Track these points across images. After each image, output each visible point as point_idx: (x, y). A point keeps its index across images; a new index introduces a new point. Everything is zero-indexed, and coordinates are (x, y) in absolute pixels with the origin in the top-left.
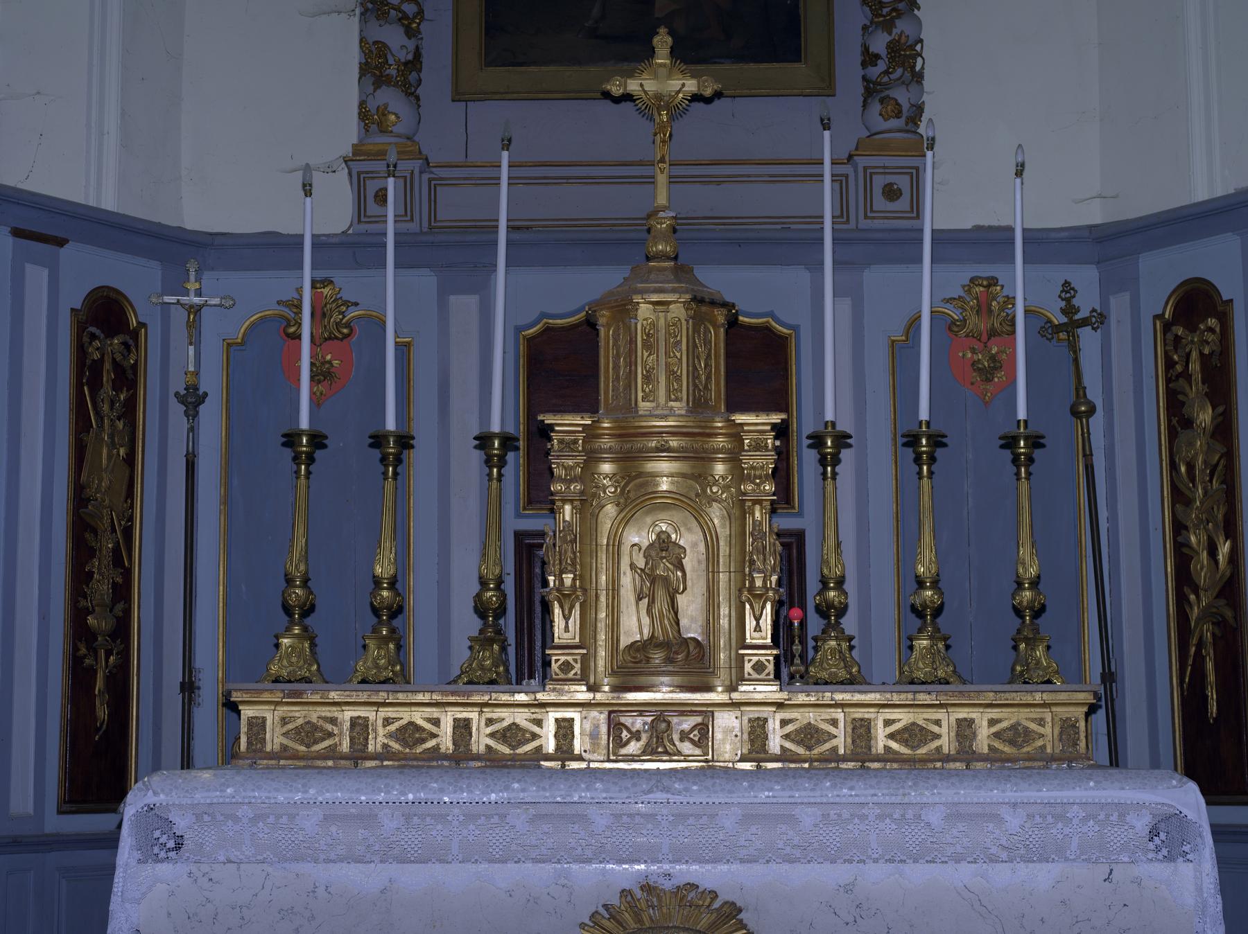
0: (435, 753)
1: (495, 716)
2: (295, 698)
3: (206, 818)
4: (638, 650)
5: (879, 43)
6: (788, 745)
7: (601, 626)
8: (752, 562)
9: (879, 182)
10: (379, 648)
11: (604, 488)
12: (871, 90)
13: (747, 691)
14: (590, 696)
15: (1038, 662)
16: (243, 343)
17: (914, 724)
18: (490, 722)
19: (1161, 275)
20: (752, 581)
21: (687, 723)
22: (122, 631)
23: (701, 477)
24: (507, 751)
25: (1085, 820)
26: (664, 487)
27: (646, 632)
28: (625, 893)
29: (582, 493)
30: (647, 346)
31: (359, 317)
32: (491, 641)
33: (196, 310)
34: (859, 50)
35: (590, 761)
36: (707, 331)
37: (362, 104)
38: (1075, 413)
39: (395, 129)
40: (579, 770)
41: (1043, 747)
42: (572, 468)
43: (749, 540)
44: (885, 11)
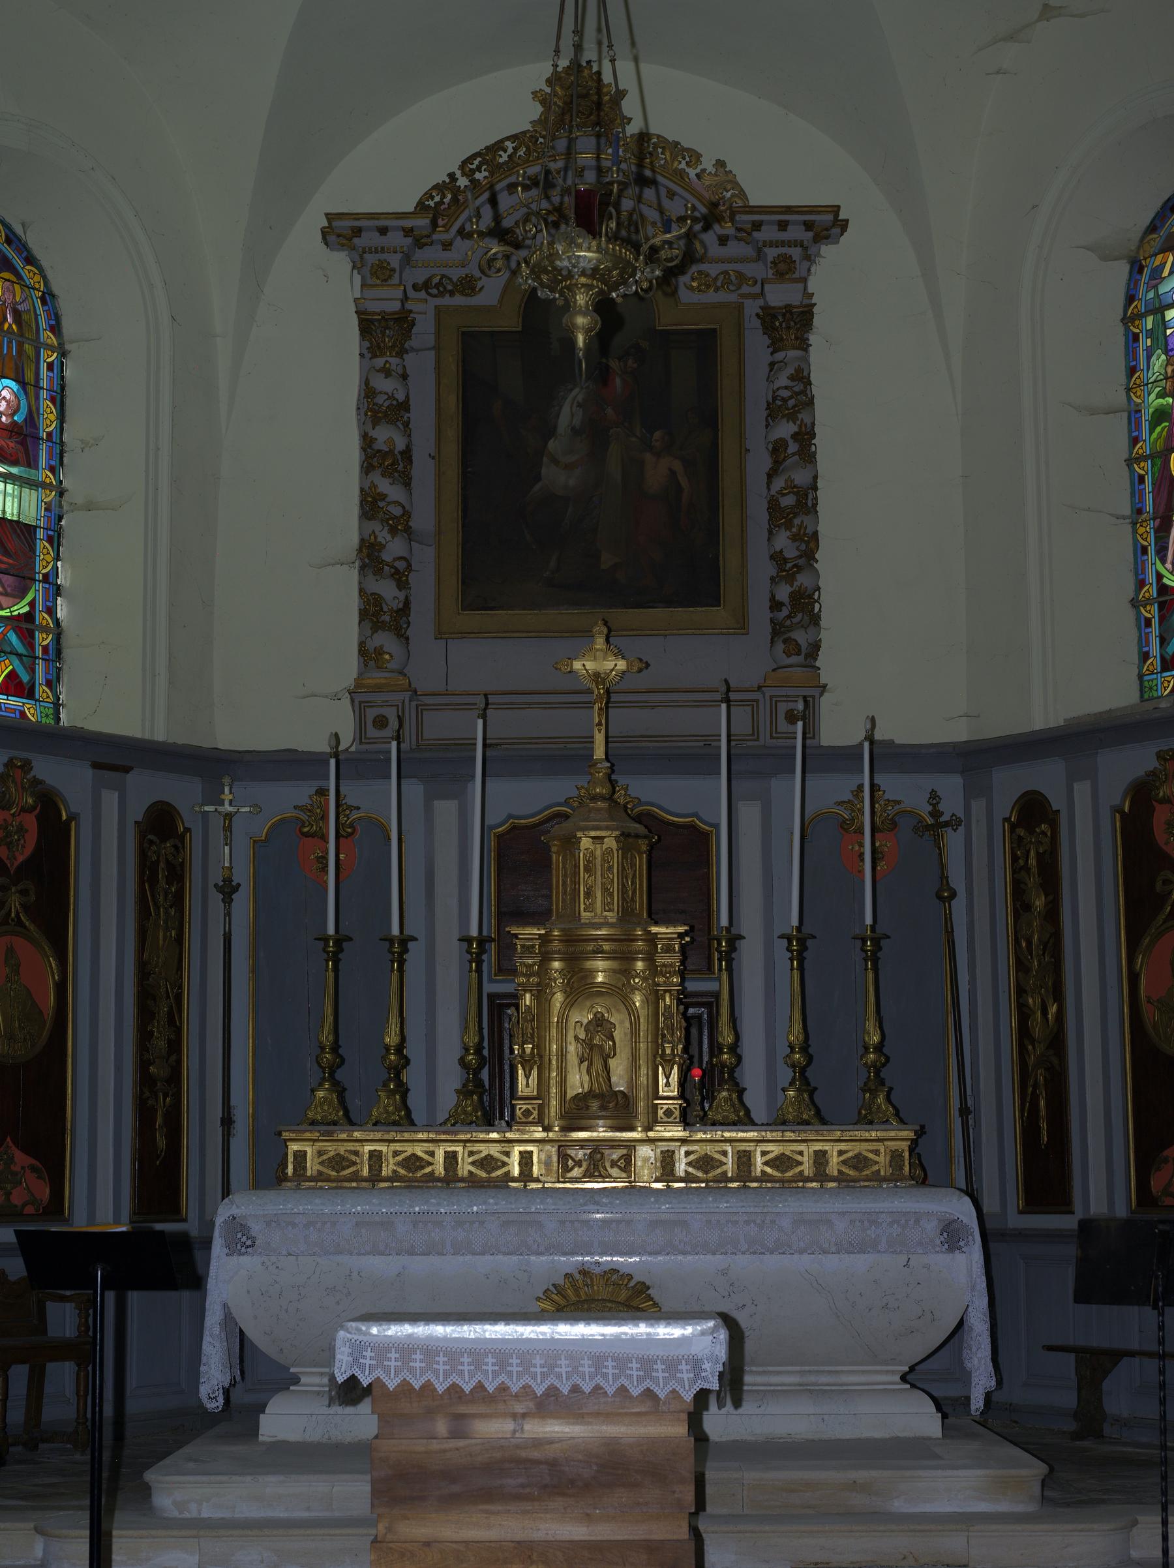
0: (431, 1177)
1: (475, 1149)
2: (328, 1136)
3: (274, 1224)
4: (580, 1100)
5: (783, 593)
6: (690, 1170)
7: (553, 1082)
8: (664, 1036)
9: (782, 708)
10: (388, 1098)
11: (555, 980)
12: (778, 630)
13: (661, 1132)
14: (544, 1135)
15: (879, 1107)
16: (267, 840)
17: (783, 1154)
18: (471, 1153)
19: (1009, 784)
20: (664, 1050)
21: (616, 1155)
22: (175, 1077)
23: (626, 972)
24: (484, 1175)
25: (891, 1224)
26: (600, 979)
27: (586, 1086)
28: (568, 1276)
29: (538, 984)
30: (587, 869)
31: (360, 819)
32: (471, 1093)
33: (229, 816)
34: (768, 596)
35: (545, 1182)
36: (633, 857)
37: (362, 645)
38: (940, 898)
39: (388, 665)
40: (537, 1189)
41: (879, 1171)
42: (532, 966)
43: (662, 1019)
44: (789, 565)
